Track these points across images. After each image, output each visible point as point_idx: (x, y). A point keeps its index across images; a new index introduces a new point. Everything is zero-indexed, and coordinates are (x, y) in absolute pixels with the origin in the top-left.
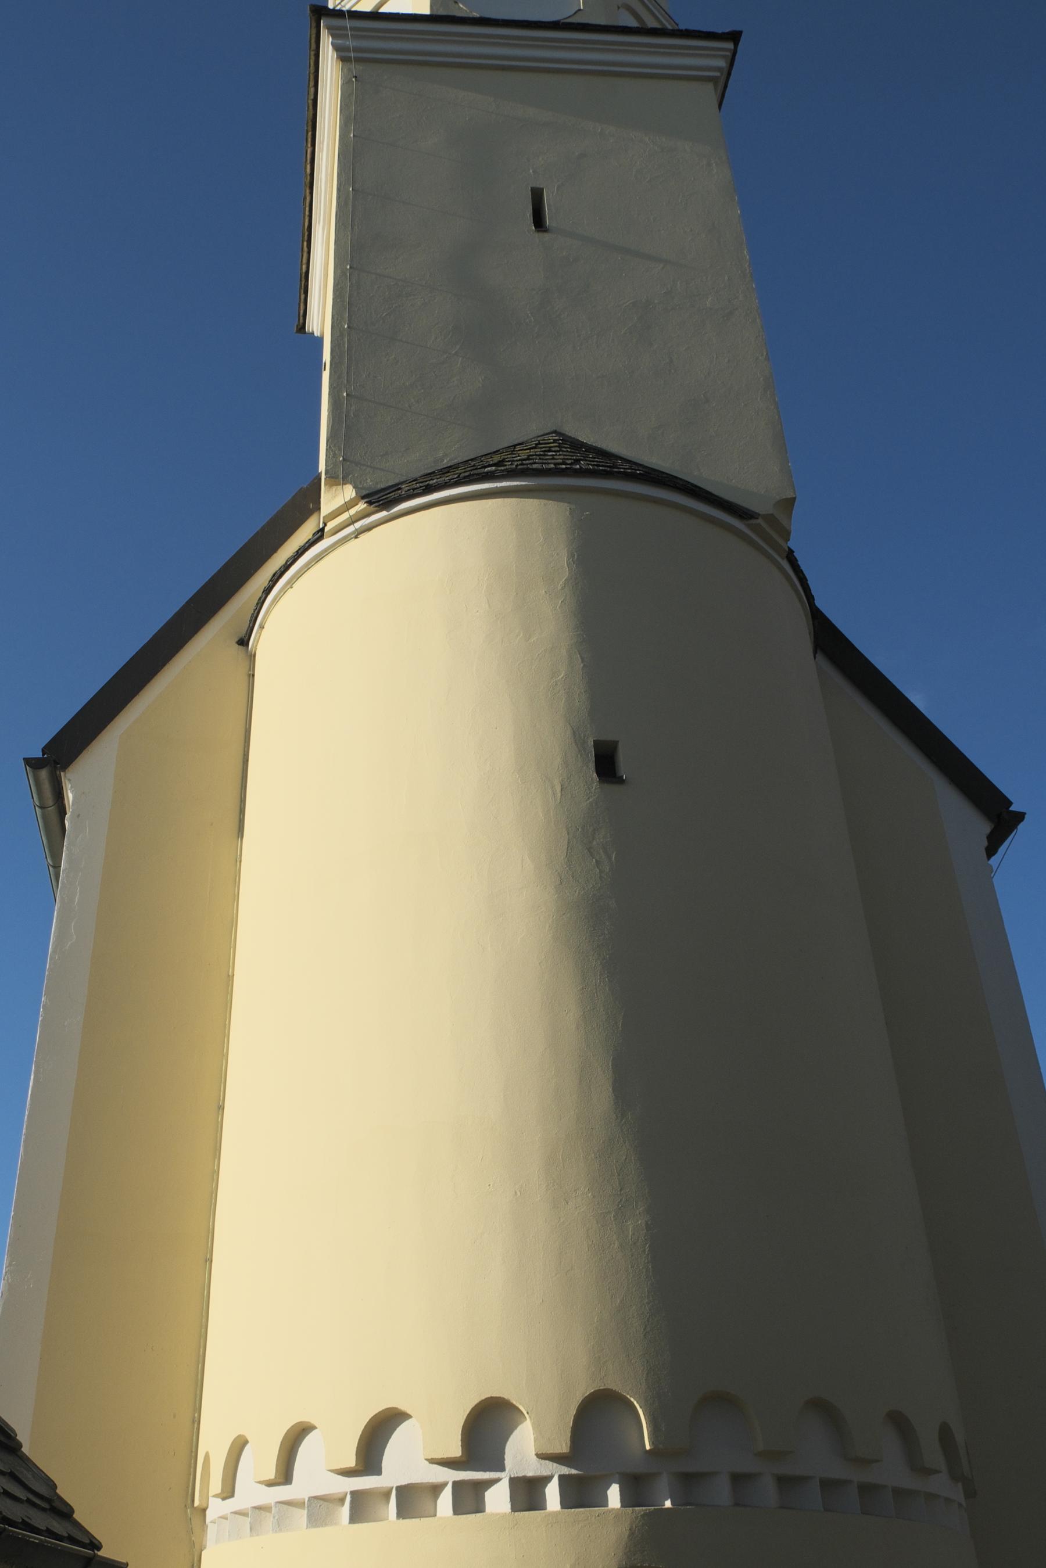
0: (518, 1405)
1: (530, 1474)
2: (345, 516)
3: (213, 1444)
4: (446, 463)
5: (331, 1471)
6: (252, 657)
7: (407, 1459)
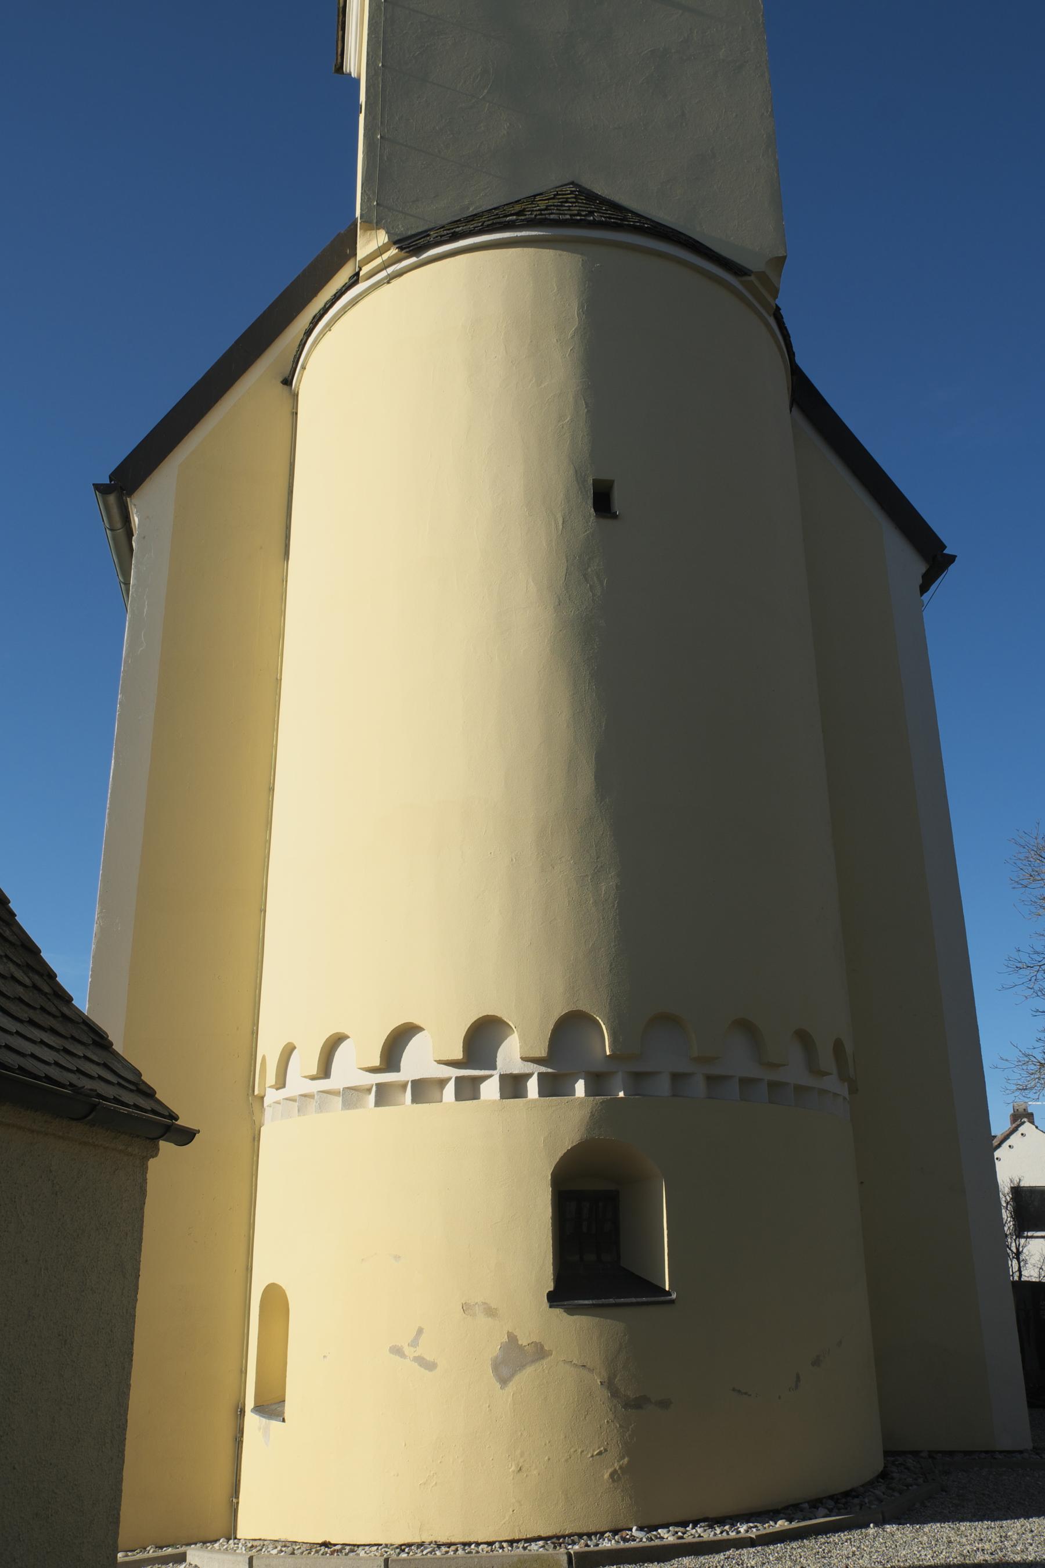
1: (516, 1072)
2: (378, 261)
3: (268, 1050)
4: (472, 211)
6: (295, 396)
7: (420, 1060)
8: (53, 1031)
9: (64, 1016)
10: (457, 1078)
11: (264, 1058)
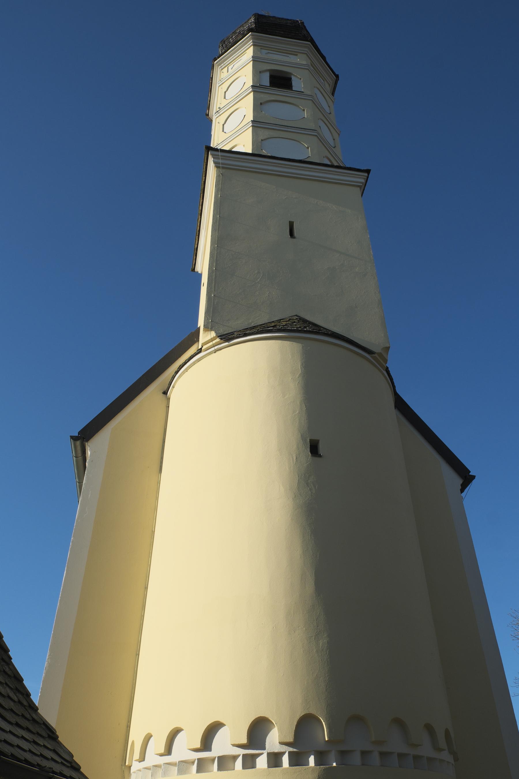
0: (272, 720)
1: (276, 751)
2: (211, 344)
3: (136, 737)
4: (253, 325)
5: (189, 749)
6: (168, 399)
7: (224, 744)
8: (28, 730)
9: (34, 720)
10: (243, 755)
11: (133, 742)
